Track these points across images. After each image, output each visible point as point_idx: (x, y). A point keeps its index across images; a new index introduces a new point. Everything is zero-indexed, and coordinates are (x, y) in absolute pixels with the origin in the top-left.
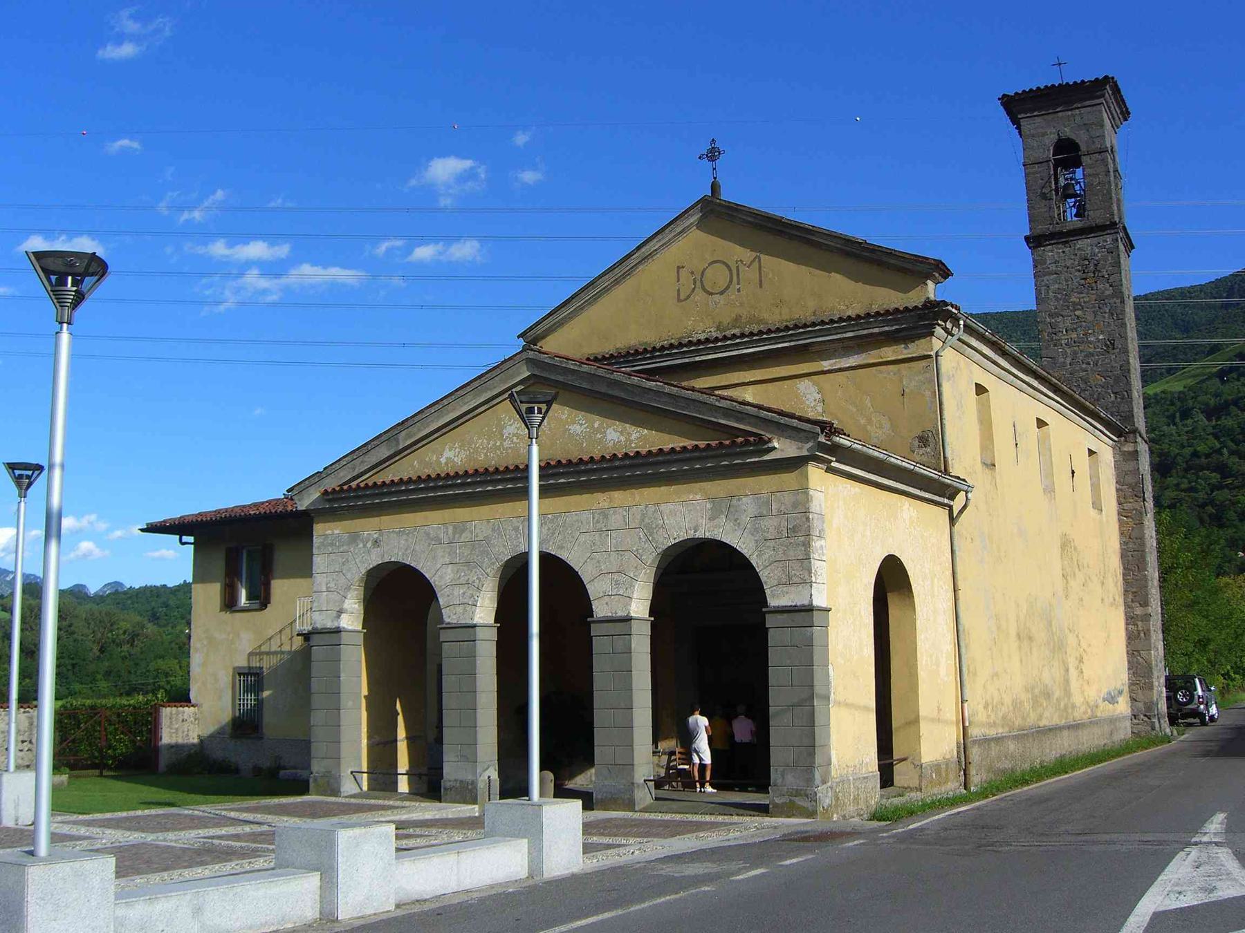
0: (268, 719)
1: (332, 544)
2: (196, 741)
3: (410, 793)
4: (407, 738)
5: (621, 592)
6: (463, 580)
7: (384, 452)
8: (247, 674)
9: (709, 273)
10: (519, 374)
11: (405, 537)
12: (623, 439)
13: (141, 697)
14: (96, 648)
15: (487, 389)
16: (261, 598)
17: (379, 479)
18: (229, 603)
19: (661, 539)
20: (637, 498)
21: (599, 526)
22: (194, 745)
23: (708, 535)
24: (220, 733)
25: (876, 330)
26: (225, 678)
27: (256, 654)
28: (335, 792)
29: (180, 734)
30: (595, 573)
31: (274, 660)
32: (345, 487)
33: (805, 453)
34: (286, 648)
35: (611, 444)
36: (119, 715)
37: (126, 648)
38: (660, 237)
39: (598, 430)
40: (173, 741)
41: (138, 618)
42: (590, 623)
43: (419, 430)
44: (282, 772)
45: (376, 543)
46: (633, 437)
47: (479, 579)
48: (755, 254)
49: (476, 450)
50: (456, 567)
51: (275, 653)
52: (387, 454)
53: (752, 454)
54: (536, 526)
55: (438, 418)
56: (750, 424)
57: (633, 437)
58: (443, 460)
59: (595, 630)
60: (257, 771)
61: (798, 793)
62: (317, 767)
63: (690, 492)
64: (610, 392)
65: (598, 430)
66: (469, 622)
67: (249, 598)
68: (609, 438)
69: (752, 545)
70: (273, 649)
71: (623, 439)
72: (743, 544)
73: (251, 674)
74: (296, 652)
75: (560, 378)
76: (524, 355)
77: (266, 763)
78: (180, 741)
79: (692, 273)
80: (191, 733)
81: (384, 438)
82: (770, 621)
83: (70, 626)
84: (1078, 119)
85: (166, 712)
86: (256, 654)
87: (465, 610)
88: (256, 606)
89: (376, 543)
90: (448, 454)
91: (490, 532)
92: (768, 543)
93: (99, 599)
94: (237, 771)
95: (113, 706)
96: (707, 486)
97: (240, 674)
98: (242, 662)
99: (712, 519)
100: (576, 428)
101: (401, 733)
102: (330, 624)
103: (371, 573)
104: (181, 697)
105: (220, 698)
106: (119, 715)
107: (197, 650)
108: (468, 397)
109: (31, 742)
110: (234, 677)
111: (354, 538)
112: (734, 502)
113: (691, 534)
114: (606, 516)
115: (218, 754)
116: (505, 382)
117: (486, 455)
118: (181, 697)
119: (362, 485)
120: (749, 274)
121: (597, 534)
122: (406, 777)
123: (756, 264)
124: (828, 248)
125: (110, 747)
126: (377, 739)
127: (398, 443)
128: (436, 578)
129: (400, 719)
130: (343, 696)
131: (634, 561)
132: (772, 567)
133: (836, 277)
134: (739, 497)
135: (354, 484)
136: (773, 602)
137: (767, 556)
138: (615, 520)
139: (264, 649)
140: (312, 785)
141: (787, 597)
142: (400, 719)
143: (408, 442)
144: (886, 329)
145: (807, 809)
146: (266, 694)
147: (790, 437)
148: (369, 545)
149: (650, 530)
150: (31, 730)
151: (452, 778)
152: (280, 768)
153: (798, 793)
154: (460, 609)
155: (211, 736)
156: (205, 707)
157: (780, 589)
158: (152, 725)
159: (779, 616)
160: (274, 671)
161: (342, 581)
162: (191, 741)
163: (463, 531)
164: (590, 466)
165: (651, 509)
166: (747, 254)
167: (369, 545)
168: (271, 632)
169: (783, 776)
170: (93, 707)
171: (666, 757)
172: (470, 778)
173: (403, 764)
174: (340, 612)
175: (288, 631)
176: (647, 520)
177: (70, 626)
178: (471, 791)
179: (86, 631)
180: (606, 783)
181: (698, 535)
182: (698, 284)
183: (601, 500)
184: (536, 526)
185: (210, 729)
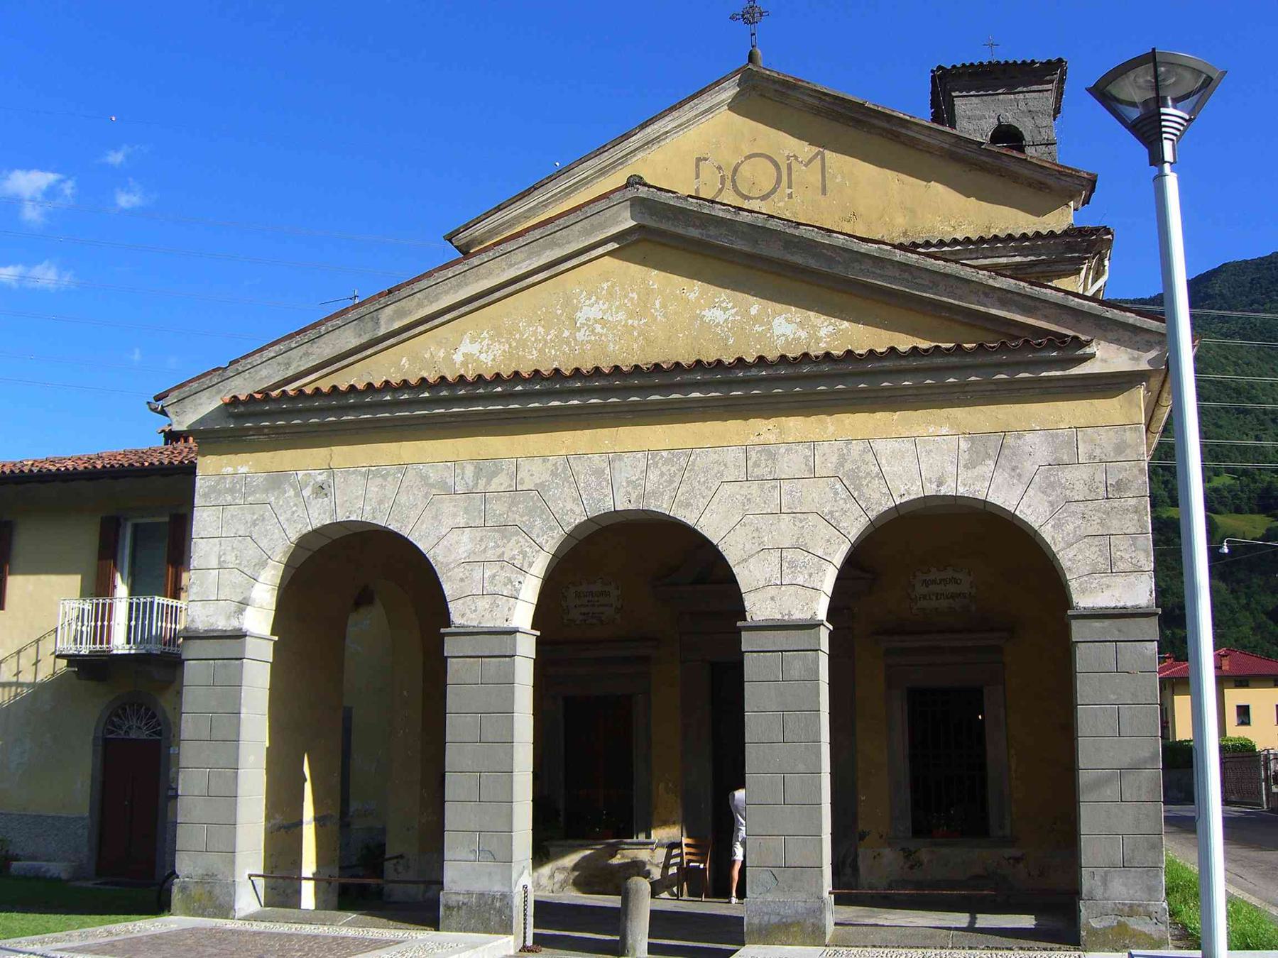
1: (231, 491)
3: (317, 908)
4: (316, 819)
5: (800, 580)
6: (491, 555)
7: (348, 339)
9: (745, 170)
10: (616, 223)
11: (379, 481)
12: (803, 335)
15: (555, 244)
17: (343, 381)
19: (876, 496)
20: (831, 429)
21: (758, 472)
23: (962, 491)
25: (1004, 260)
28: (225, 910)
30: (751, 547)
32: (274, 394)
33: (1144, 366)
34: (27, 677)
35: (781, 341)
38: (675, 114)
39: (755, 320)
42: (739, 631)
43: (420, 305)
44: (15, 864)
45: (321, 489)
46: (823, 332)
47: (524, 554)
48: (815, 149)
49: (523, 344)
50: (478, 533)
51: (9, 684)
52: (354, 342)
53: (1051, 364)
54: (626, 470)
55: (459, 286)
56: (1046, 318)
57: (823, 332)
58: (458, 358)
59: (748, 641)
61: (1132, 911)
62: (186, 866)
63: (929, 423)
64: (789, 257)
65: (755, 320)
66: (500, 624)
68: (777, 331)
69: (1044, 509)
71: (803, 335)
72: (1032, 510)
75: (694, 233)
76: (630, 193)
79: (719, 168)
81: (352, 315)
82: (1079, 631)
84: (1022, 104)
87: (494, 605)
89: (321, 489)
90: (467, 347)
91: (546, 477)
92: (1073, 507)
96: (959, 413)
99: (970, 465)
100: (715, 315)
102: (222, 624)
103: (304, 542)
108: (518, 255)
111: (277, 480)
112: (1010, 440)
113: (931, 490)
114: (773, 457)
116: (588, 233)
117: (541, 351)
119: (308, 390)
120: (812, 176)
121: (755, 485)
122: (312, 883)
123: (818, 161)
124: (928, 150)
126: (279, 819)
127: (377, 322)
128: (438, 550)
129: (308, 787)
130: (243, 746)
131: (825, 531)
132: (1081, 544)
133: (937, 187)
134: (1019, 433)
135: (289, 389)
136: (1083, 599)
137: (1070, 527)
138: (791, 463)
140: (176, 896)
141: (1107, 593)
142: (308, 787)
143: (397, 325)
144: (1018, 259)
145: (1150, 936)
147: (1118, 341)
148: (307, 492)
149: (851, 484)
151: (462, 887)
153: (1132, 911)
154: (483, 604)
157: (1096, 581)
159: (1097, 624)
161: (251, 552)
163: (495, 474)
164: (754, 372)
165: (857, 447)
166: (805, 149)
167: (307, 492)
169: (1105, 883)
171: (665, 851)
172: (497, 888)
173: (309, 865)
174: (244, 604)
176: (848, 466)
178: (500, 912)
180: (770, 897)
181: (944, 491)
182: (728, 183)
183: (763, 429)
184: (626, 470)
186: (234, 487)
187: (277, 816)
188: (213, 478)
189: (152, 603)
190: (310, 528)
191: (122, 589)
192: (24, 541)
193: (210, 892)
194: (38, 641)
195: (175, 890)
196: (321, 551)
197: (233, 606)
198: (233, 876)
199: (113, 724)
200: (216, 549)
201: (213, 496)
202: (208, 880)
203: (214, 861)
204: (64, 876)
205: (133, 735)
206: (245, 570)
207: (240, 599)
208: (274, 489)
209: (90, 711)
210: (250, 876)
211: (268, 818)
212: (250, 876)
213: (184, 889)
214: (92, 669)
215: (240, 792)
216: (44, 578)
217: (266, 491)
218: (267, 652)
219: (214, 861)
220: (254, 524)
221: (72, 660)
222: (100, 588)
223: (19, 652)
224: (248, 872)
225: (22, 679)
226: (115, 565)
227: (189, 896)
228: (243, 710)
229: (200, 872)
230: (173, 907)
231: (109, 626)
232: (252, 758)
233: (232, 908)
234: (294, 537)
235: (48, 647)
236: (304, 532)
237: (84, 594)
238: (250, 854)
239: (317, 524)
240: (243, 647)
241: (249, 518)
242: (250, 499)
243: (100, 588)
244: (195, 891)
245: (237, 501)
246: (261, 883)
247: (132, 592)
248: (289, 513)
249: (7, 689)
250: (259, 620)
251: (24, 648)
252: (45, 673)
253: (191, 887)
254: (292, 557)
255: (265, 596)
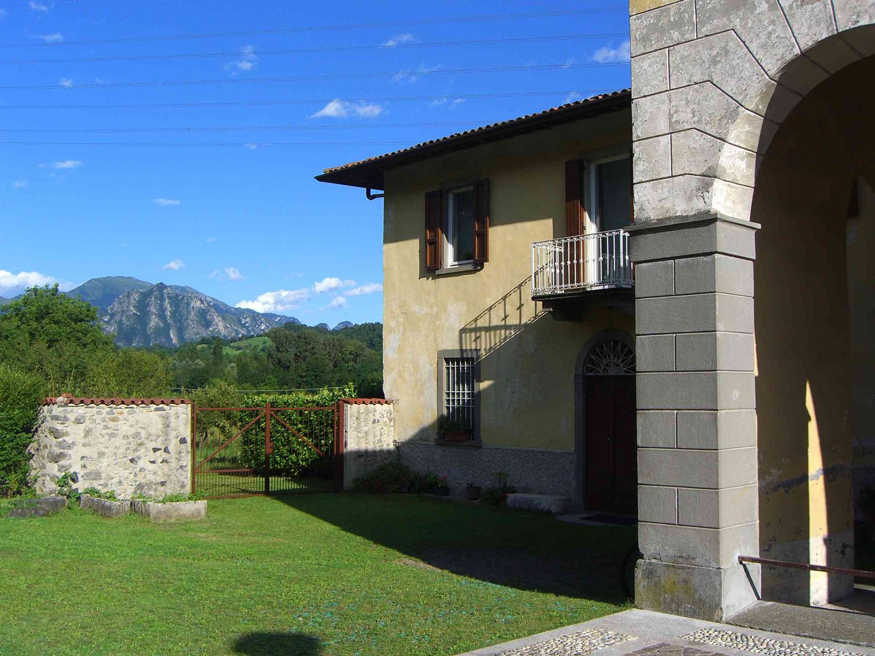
0: (487, 418)
1: (678, 25)
2: (392, 447)
8: (458, 360)
13: (325, 392)
14: (331, 365)
16: (474, 256)
18: (431, 267)
22: (389, 452)
24: (422, 436)
26: (427, 366)
27: (471, 330)
28: (706, 607)
29: (371, 438)
31: (495, 339)
34: (513, 321)
36: (301, 413)
37: (351, 364)
40: (363, 446)
41: (360, 343)
44: (511, 497)
51: (496, 328)
60: (474, 491)
62: (652, 542)
67: (458, 257)
70: (493, 324)
73: (463, 359)
74: (526, 325)
77: (486, 483)
78: (370, 447)
80: (384, 438)
83: (313, 348)
85: (352, 411)
86: (471, 330)
88: (470, 267)
93: (335, 332)
94: (446, 491)
95: (295, 403)
97: (447, 360)
98: (451, 344)
101: (815, 462)
104: (372, 392)
105: (422, 392)
106: (301, 413)
107: (391, 330)
109: (166, 450)
110: (439, 365)
115: (419, 466)
118: (372, 392)
125: (292, 451)
126: (776, 474)
130: (722, 378)
139: (480, 324)
146: (484, 385)
150: (166, 434)
152: (508, 489)
155: (411, 443)
156: (403, 404)
158: (333, 423)
160: (496, 353)
161: (714, 101)
162: (385, 447)
168: (489, 302)
170: (273, 404)
174: (709, 176)
175: (515, 297)
177: (313, 348)
179: (323, 352)
185: (407, 433)
186: (681, 19)
187: (774, 471)
188: (651, 14)
189: (618, 237)
190: (797, 51)
191: (591, 227)
192: (502, 195)
193: (685, 582)
194: (520, 285)
195: (639, 573)
196: (819, 91)
197: (694, 182)
198: (717, 560)
199: (592, 361)
200: (665, 108)
201: (653, 37)
202: (683, 563)
203: (689, 539)
204: (554, 509)
205: (612, 372)
206: (708, 129)
207: (702, 170)
208: (738, 8)
209: (570, 349)
210: (741, 560)
211: (763, 473)
212: (741, 560)
213: (650, 573)
214: (567, 307)
215: (722, 444)
216: (520, 226)
217: (726, 12)
218: (748, 245)
219: (689, 539)
220: (714, 62)
221: (547, 300)
222: (570, 228)
223: (504, 298)
224: (738, 554)
225: (509, 322)
226: (582, 205)
227: (657, 584)
228: (720, 326)
229: (671, 552)
230: (637, 597)
231: (578, 264)
232: (736, 394)
233: (718, 606)
234: (773, 67)
235: (529, 291)
236: (789, 57)
237: (556, 235)
238: (740, 532)
239: (807, 41)
240: (713, 238)
241: (705, 55)
242: (704, 30)
243: (570, 228)
244: (666, 578)
245: (688, 36)
246: (756, 569)
247: (602, 228)
248: (763, 36)
249: (498, 332)
250: (732, 199)
251: (509, 294)
252: (528, 316)
253: (660, 571)
254: (774, 104)
255: (738, 162)
